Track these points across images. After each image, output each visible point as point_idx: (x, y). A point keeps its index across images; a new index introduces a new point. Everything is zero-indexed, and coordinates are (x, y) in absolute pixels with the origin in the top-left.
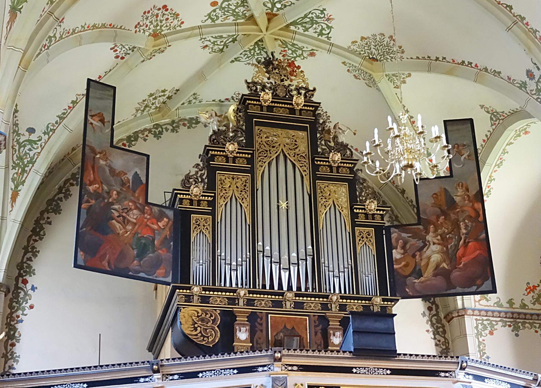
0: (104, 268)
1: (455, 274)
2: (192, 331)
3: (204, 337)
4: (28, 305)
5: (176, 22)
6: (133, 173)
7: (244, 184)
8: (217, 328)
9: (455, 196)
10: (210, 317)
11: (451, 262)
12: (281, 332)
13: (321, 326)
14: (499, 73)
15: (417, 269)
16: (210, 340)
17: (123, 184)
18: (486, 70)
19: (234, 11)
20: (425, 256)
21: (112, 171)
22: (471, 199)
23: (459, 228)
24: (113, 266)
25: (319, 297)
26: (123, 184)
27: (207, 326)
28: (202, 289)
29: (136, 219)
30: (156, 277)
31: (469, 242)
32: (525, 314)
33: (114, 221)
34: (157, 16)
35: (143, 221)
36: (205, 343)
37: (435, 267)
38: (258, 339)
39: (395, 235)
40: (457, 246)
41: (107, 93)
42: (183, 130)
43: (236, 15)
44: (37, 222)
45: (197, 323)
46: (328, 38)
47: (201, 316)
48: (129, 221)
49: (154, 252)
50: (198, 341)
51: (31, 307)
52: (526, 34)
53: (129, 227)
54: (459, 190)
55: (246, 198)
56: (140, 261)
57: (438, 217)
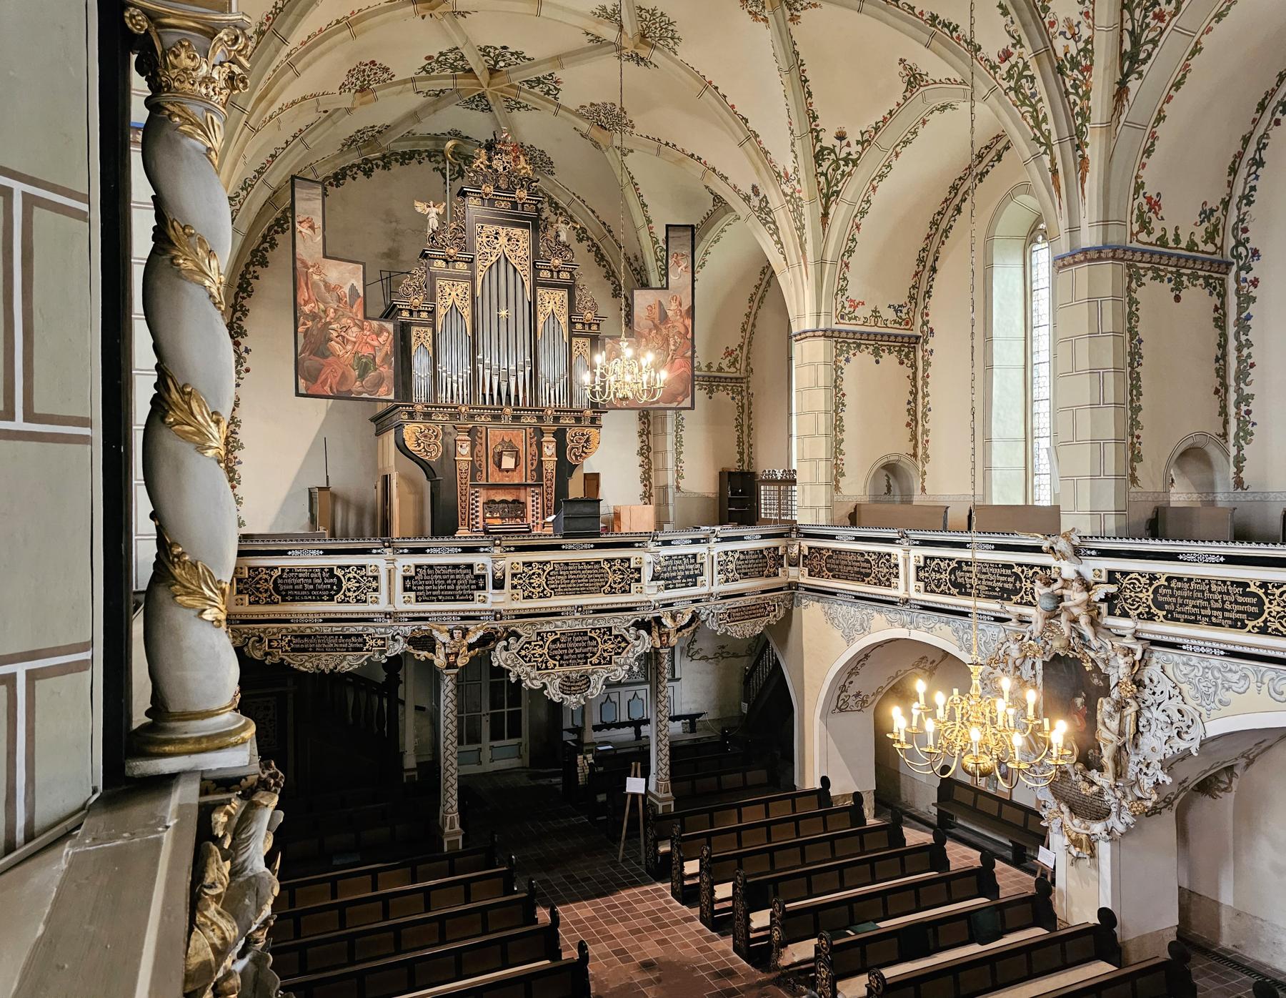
4: (243, 368)
5: (385, 75)
6: (349, 285)
14: (726, 178)
17: (340, 299)
18: (714, 170)
19: (452, 64)
21: (327, 285)
23: (668, 344)
25: (535, 411)
26: (340, 299)
32: (720, 378)
34: (364, 71)
41: (314, 191)
42: (395, 167)
43: (454, 68)
44: (243, 276)
46: (555, 98)
48: (348, 340)
49: (376, 369)
51: (247, 370)
52: (757, 153)
53: (349, 347)
57: (650, 331)
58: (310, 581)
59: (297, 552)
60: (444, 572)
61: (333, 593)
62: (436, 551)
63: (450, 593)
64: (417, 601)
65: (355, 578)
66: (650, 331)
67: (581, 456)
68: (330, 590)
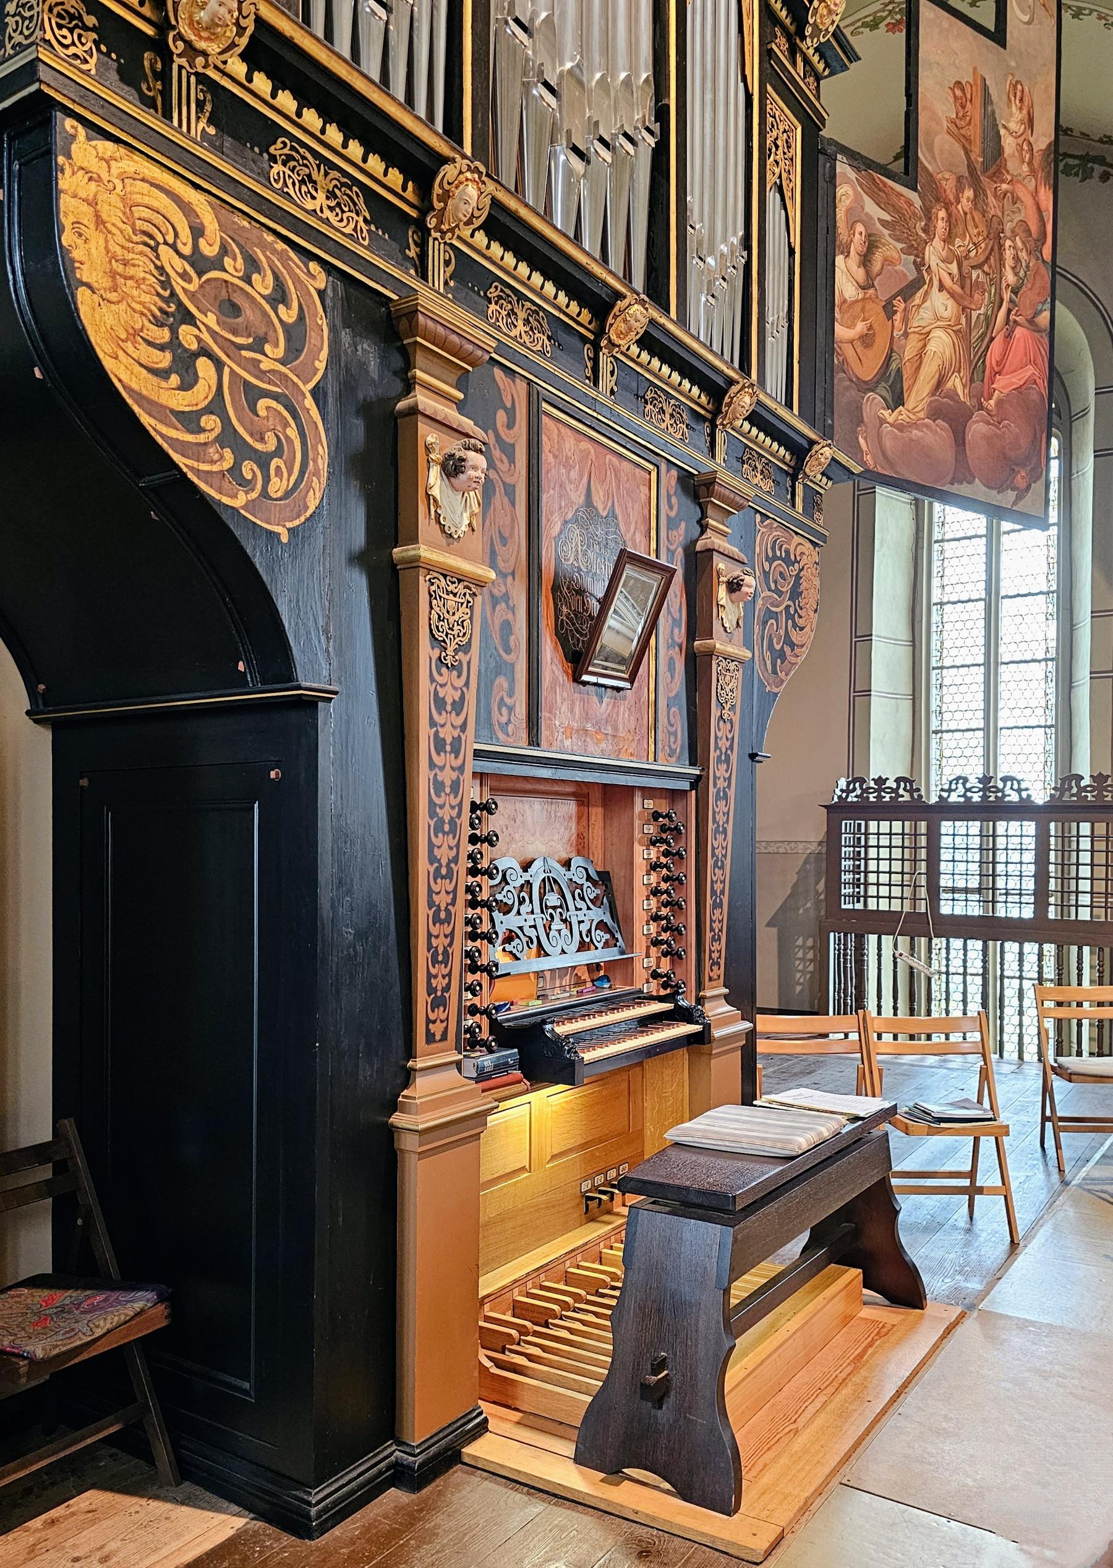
1: (977, 428)
3: (243, 451)
8: (309, 402)
9: (1005, 127)
11: (972, 380)
15: (894, 366)
16: (277, 486)
22: (1036, 163)
36: (249, 506)
37: (935, 380)
45: (190, 320)
57: (960, 189)
66: (960, 189)
67: (782, 655)
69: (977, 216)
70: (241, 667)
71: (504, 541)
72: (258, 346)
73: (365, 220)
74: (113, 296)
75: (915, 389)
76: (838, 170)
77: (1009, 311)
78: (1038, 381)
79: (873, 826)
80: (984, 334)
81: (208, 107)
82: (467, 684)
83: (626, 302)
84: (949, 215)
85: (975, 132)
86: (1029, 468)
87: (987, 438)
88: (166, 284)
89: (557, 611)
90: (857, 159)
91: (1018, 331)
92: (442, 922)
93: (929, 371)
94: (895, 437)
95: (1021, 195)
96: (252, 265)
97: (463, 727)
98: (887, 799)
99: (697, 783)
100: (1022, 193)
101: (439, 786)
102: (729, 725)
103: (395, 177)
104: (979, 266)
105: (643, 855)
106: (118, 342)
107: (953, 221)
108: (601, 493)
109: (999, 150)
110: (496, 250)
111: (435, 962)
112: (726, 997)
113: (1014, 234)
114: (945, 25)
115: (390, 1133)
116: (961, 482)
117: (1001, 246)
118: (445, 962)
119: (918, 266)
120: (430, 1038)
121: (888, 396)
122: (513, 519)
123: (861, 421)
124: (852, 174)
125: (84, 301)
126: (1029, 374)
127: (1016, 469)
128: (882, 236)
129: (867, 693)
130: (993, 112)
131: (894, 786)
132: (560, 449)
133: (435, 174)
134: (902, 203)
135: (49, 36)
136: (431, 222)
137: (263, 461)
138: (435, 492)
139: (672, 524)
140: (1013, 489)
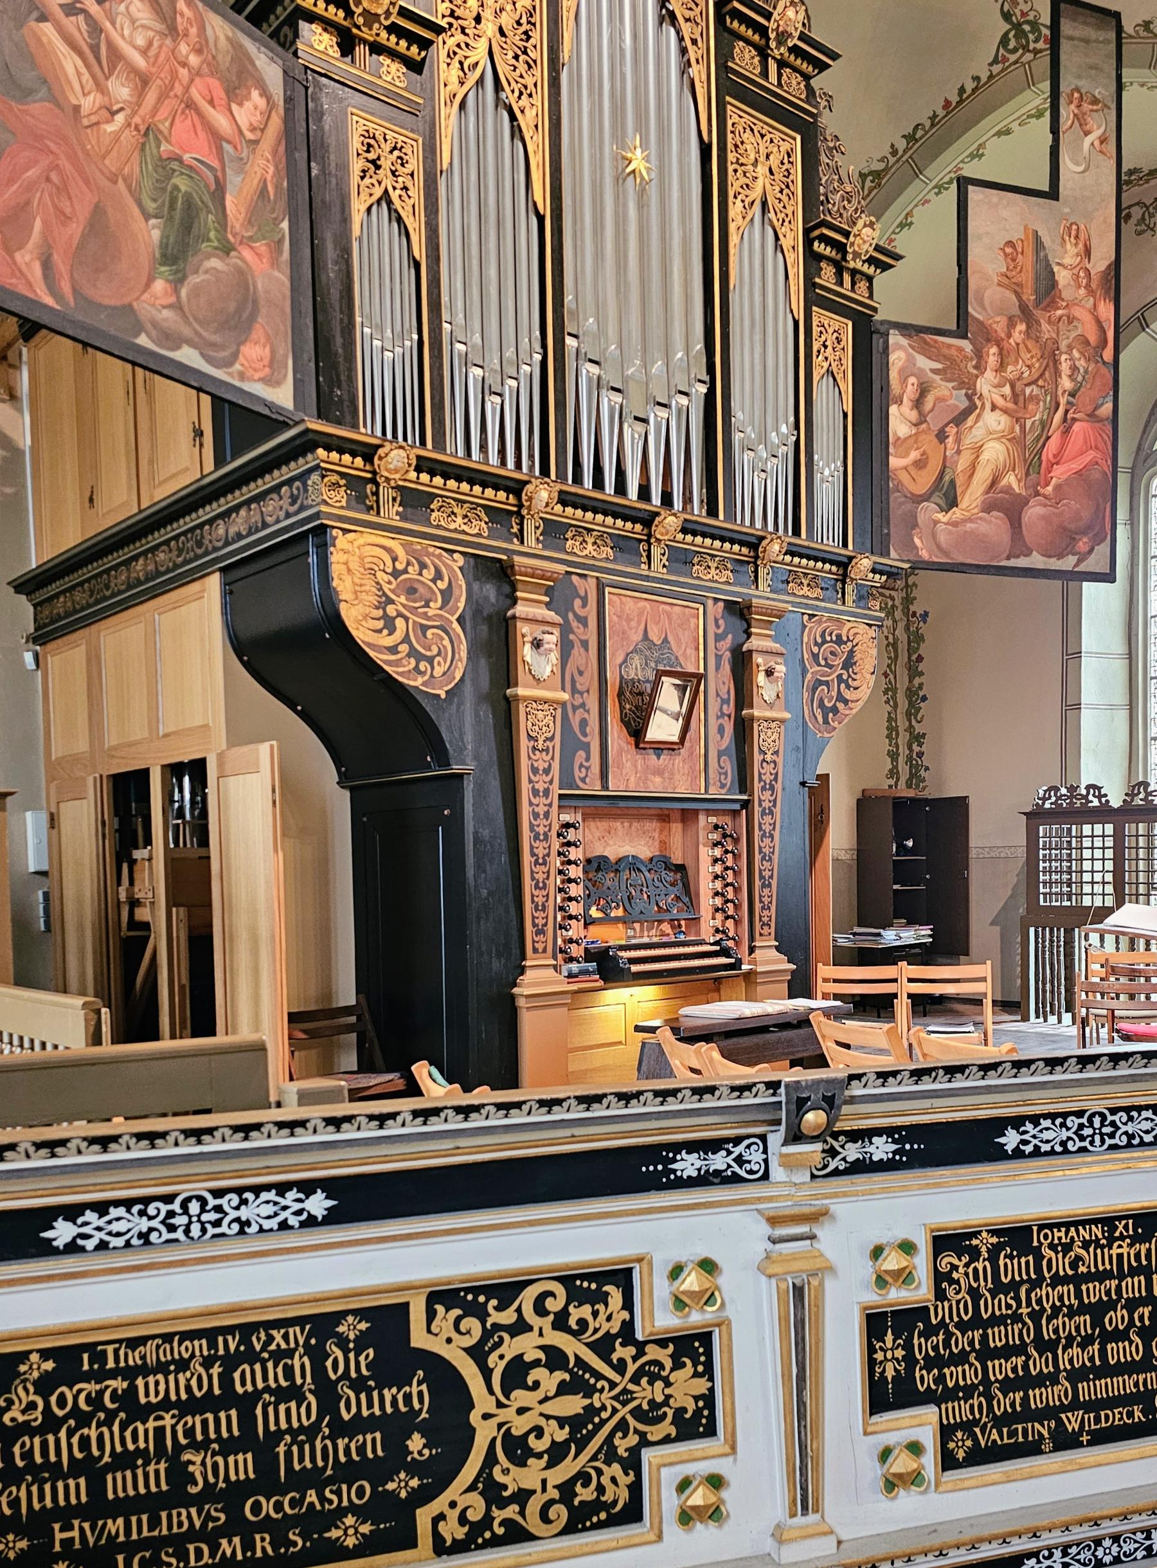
0: (23, 290)
1: (1034, 512)
2: (380, 631)
3: (419, 657)
7: (525, 27)
8: (456, 625)
9: (1058, 264)
10: (434, 581)
11: (1027, 474)
12: (635, 651)
13: (730, 636)
15: (947, 478)
16: (438, 671)
20: (967, 441)
22: (1094, 285)
23: (1057, 373)
24: (66, 287)
27: (425, 616)
28: (414, 462)
29: (144, 52)
30: (242, 376)
31: (1074, 420)
33: (47, 28)
35: (174, 75)
36: (424, 684)
37: (989, 482)
38: (577, 677)
39: (899, 359)
40: (1045, 425)
45: (392, 602)
47: (405, 571)
49: (226, 249)
50: (397, 673)
54: (1068, 246)
55: (530, 95)
56: (178, 281)
57: (1011, 324)
58: (229, 1421)
59: (131, 1223)
60: (1090, 1260)
61: (402, 1485)
62: (1052, 1134)
63: (1126, 1384)
64: (948, 1462)
65: (554, 1358)
66: (1011, 324)
67: (835, 710)
68: (379, 1471)
69: (1030, 344)
70: (429, 759)
71: (581, 673)
72: (427, 605)
73: (486, 523)
74: (356, 602)
75: (969, 491)
76: (891, 342)
77: (1067, 411)
78: (1100, 462)
79: (1087, 830)
80: (1040, 436)
81: (399, 499)
82: (553, 758)
83: (662, 517)
84: (1001, 350)
85: (1027, 278)
86: (1091, 535)
87: (1043, 517)
88: (381, 589)
89: (622, 708)
90: (906, 329)
91: (1077, 426)
92: (540, 889)
93: (982, 477)
94: (950, 533)
95: (1077, 314)
96: (423, 566)
97: (551, 782)
98: (1078, 805)
99: (746, 804)
100: (1077, 312)
101: (536, 815)
102: (772, 765)
103: (502, 495)
104: (1034, 382)
105: (706, 854)
106: (358, 622)
107: (1005, 352)
108: (656, 631)
109: (1053, 284)
110: (569, 510)
111: (537, 909)
112: (777, 948)
113: (1070, 348)
114: (995, 200)
115: (513, 998)
116: (1018, 557)
117: (1056, 362)
118: (544, 910)
119: (969, 397)
120: (535, 950)
121: (942, 502)
122: (587, 658)
123: (915, 525)
124: (904, 341)
125: (344, 610)
126: (1089, 459)
127: (1077, 537)
128: (934, 381)
129: (1077, 707)
130: (1046, 256)
131: (1084, 792)
132: (622, 611)
133: (522, 490)
134: (954, 352)
135: (325, 497)
136: (524, 512)
137: (430, 661)
138: (528, 658)
139: (718, 638)
140: (1073, 555)
